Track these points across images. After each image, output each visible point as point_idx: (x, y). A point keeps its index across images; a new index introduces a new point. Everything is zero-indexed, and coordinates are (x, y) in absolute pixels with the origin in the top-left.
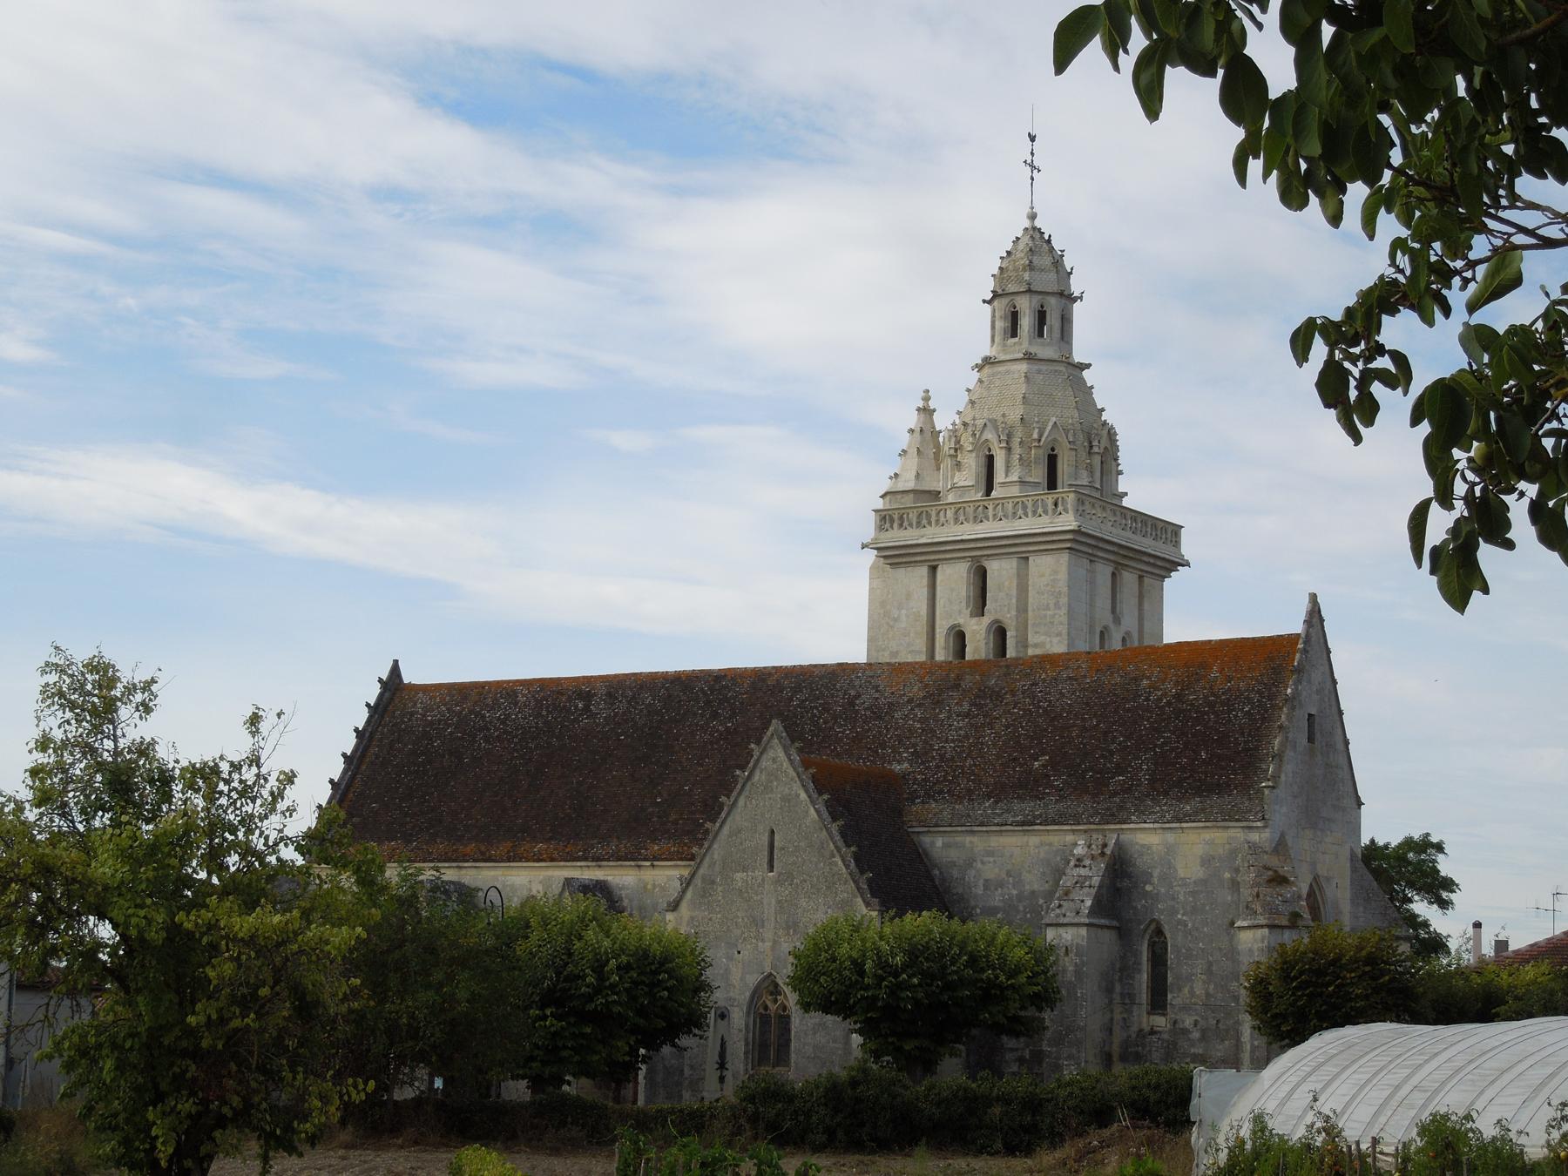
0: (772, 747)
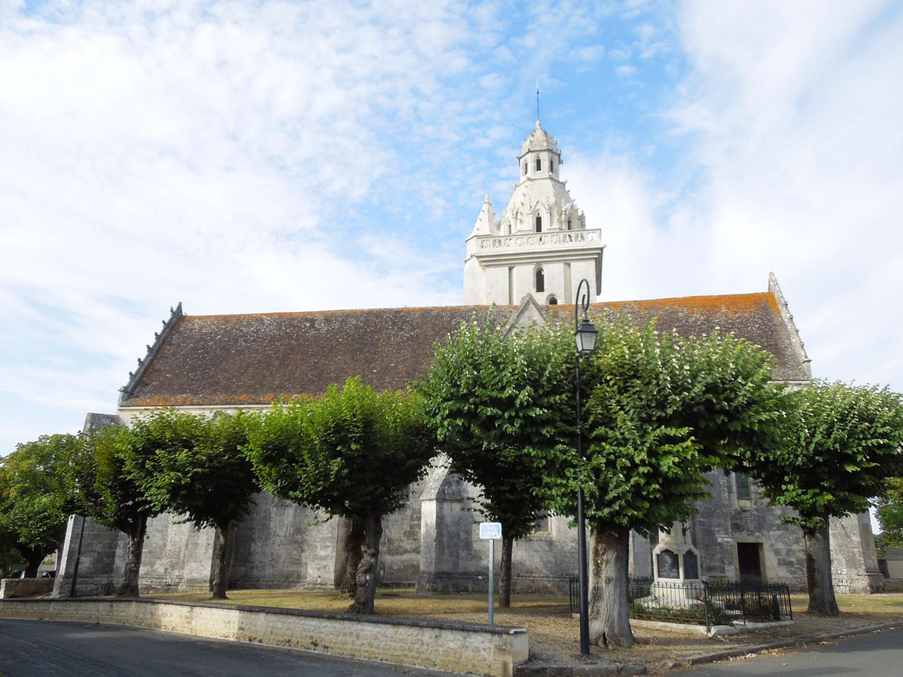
0: (529, 308)
